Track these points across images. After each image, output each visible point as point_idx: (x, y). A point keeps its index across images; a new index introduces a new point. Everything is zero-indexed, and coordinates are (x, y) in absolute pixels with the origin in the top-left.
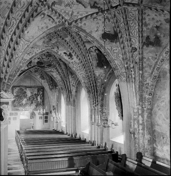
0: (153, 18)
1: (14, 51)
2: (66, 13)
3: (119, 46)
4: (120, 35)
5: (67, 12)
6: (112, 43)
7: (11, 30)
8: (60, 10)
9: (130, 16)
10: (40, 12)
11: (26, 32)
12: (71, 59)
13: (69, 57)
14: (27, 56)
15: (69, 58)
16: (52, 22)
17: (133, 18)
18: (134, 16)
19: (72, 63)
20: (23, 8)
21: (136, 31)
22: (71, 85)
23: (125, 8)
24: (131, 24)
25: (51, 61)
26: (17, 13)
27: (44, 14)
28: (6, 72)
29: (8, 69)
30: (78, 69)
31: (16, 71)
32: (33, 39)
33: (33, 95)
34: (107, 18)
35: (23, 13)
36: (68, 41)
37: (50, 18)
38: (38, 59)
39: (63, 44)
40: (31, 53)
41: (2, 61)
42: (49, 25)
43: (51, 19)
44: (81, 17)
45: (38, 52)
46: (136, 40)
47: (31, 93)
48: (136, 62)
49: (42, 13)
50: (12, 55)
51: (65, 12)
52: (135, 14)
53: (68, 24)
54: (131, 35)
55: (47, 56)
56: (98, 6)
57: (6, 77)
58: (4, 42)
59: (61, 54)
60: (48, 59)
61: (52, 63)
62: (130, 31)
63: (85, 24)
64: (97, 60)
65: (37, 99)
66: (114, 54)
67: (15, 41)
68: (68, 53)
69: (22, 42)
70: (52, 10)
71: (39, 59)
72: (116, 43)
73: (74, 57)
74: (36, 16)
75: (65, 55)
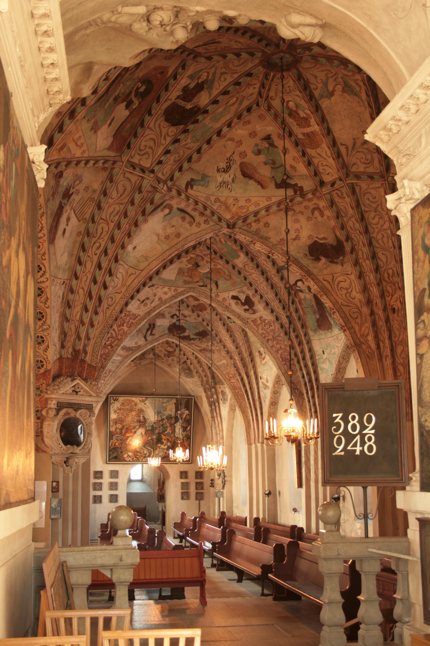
0: (267, 223)
1: (105, 289)
2: (221, 202)
3: (350, 273)
4: (348, 247)
5: (223, 199)
6: (334, 265)
7: (98, 244)
8: (205, 195)
9: (367, 202)
10: (160, 203)
11: (130, 248)
12: (251, 311)
13: (247, 307)
14: (139, 308)
15: (246, 310)
16: (191, 224)
17: (374, 206)
18: (376, 200)
19: (254, 321)
20: (122, 197)
21: (385, 235)
22: (261, 384)
23: (352, 183)
24: (373, 219)
25: (205, 323)
26: (111, 210)
27: (170, 207)
28: (88, 338)
29: (91, 331)
30: (270, 337)
31: (114, 345)
32: (147, 263)
33: (162, 420)
34: (317, 208)
35: (122, 207)
36: (240, 265)
37: (183, 214)
38: (172, 317)
39: (228, 276)
40: (148, 298)
41: (79, 314)
42: (182, 230)
43: (187, 217)
44: (268, 203)
45: (166, 297)
46: (389, 255)
47: (158, 413)
48: (394, 309)
49: (164, 205)
50: (100, 300)
51: (217, 200)
52: (377, 196)
53: (226, 226)
54: (375, 243)
55: (194, 309)
56: (293, 183)
57: (87, 349)
58: (83, 272)
59: (224, 300)
60: (198, 316)
61: (209, 328)
62: (371, 235)
63: (267, 225)
64: (314, 313)
65: (174, 431)
66: (341, 292)
67: (106, 269)
68: (243, 298)
69: (121, 270)
70: (188, 198)
71: (175, 317)
72: (342, 265)
73: (259, 307)
74: (153, 211)
75: (235, 301)
